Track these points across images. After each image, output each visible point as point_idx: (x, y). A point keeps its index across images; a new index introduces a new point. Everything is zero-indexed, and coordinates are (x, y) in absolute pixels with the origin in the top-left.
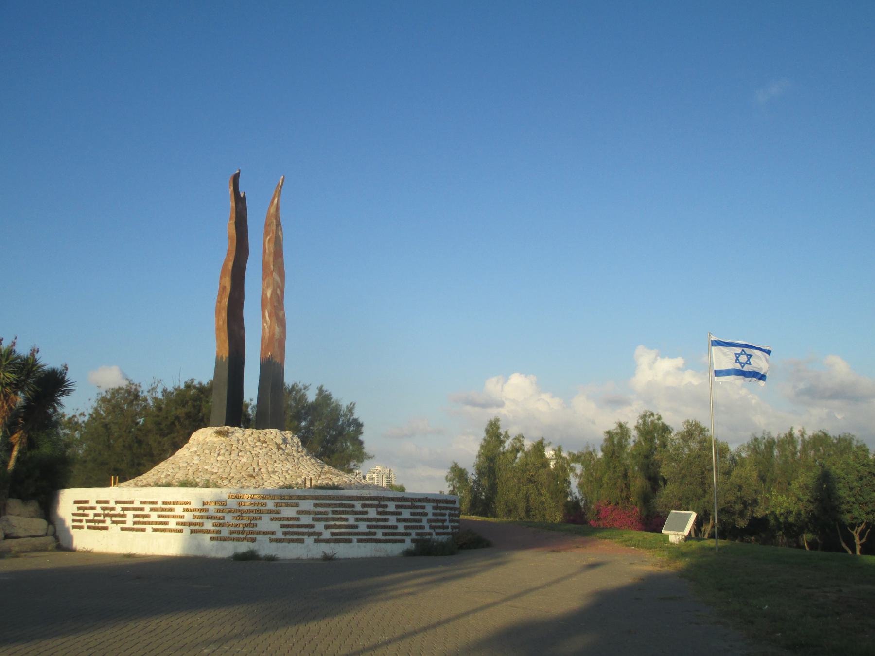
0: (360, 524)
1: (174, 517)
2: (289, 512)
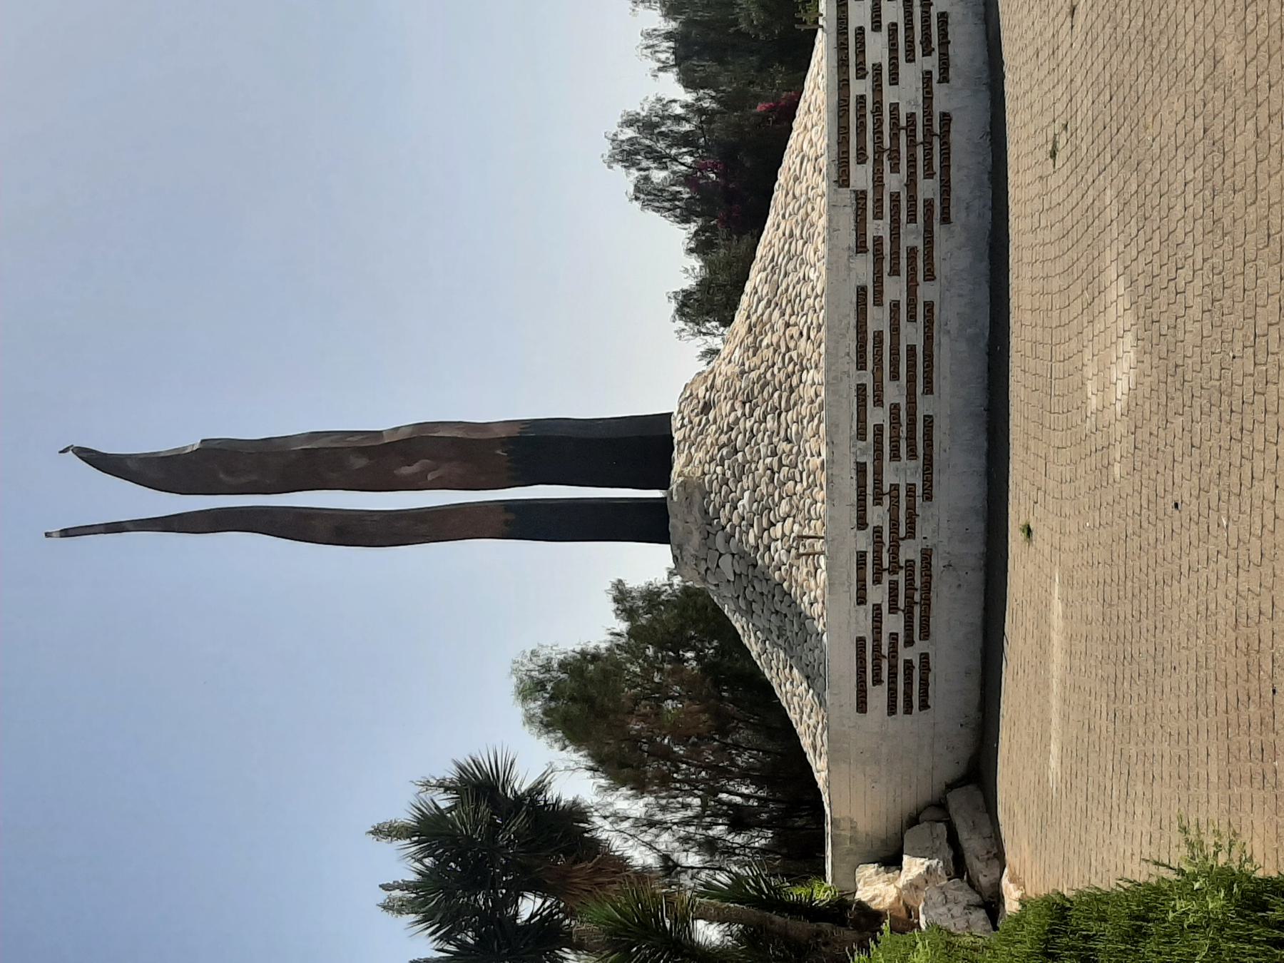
0: (888, 400)
1: (895, 330)
2: (877, 49)
